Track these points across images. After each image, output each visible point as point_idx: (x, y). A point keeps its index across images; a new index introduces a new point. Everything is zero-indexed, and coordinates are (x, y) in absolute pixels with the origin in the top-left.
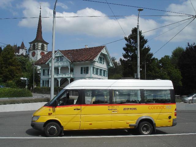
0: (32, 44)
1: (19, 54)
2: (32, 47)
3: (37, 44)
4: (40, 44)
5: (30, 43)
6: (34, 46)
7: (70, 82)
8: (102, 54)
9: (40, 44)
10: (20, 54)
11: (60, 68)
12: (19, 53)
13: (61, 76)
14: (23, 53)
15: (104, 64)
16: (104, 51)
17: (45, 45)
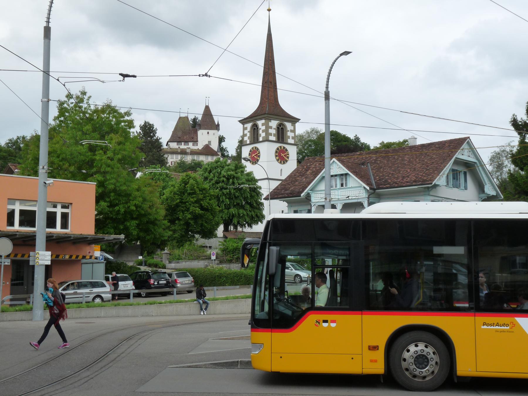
0: (249, 126)
1: (195, 148)
2: (248, 135)
3: (263, 125)
4: (274, 124)
5: (244, 121)
6: (255, 129)
7: (269, 194)
8: (458, 162)
9: (274, 124)
10: (200, 146)
11: (143, 264)
12: (195, 141)
13: (473, 280)
14: (210, 142)
15: (466, 188)
16: (463, 155)
17: (289, 126)
